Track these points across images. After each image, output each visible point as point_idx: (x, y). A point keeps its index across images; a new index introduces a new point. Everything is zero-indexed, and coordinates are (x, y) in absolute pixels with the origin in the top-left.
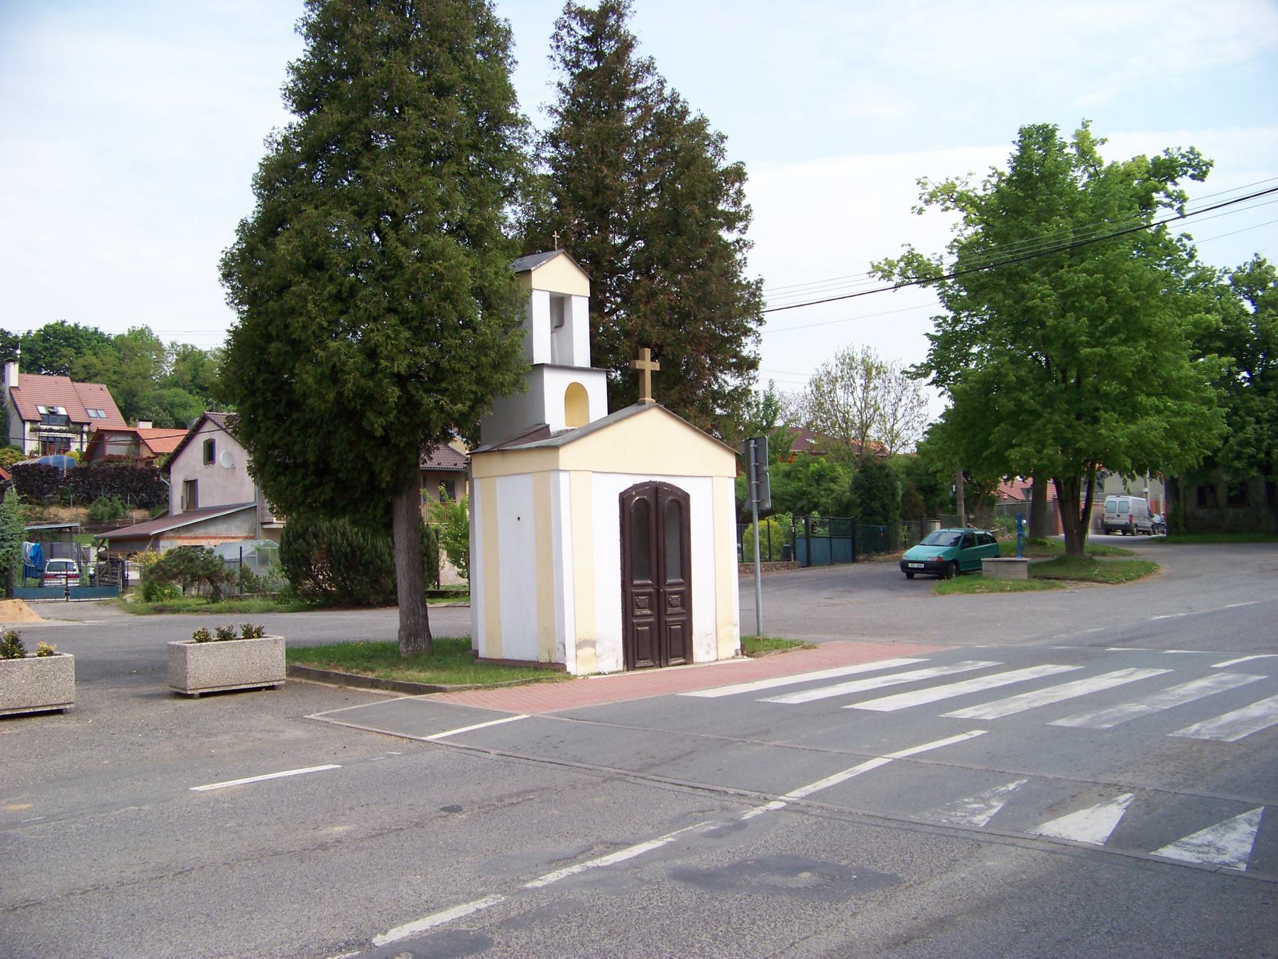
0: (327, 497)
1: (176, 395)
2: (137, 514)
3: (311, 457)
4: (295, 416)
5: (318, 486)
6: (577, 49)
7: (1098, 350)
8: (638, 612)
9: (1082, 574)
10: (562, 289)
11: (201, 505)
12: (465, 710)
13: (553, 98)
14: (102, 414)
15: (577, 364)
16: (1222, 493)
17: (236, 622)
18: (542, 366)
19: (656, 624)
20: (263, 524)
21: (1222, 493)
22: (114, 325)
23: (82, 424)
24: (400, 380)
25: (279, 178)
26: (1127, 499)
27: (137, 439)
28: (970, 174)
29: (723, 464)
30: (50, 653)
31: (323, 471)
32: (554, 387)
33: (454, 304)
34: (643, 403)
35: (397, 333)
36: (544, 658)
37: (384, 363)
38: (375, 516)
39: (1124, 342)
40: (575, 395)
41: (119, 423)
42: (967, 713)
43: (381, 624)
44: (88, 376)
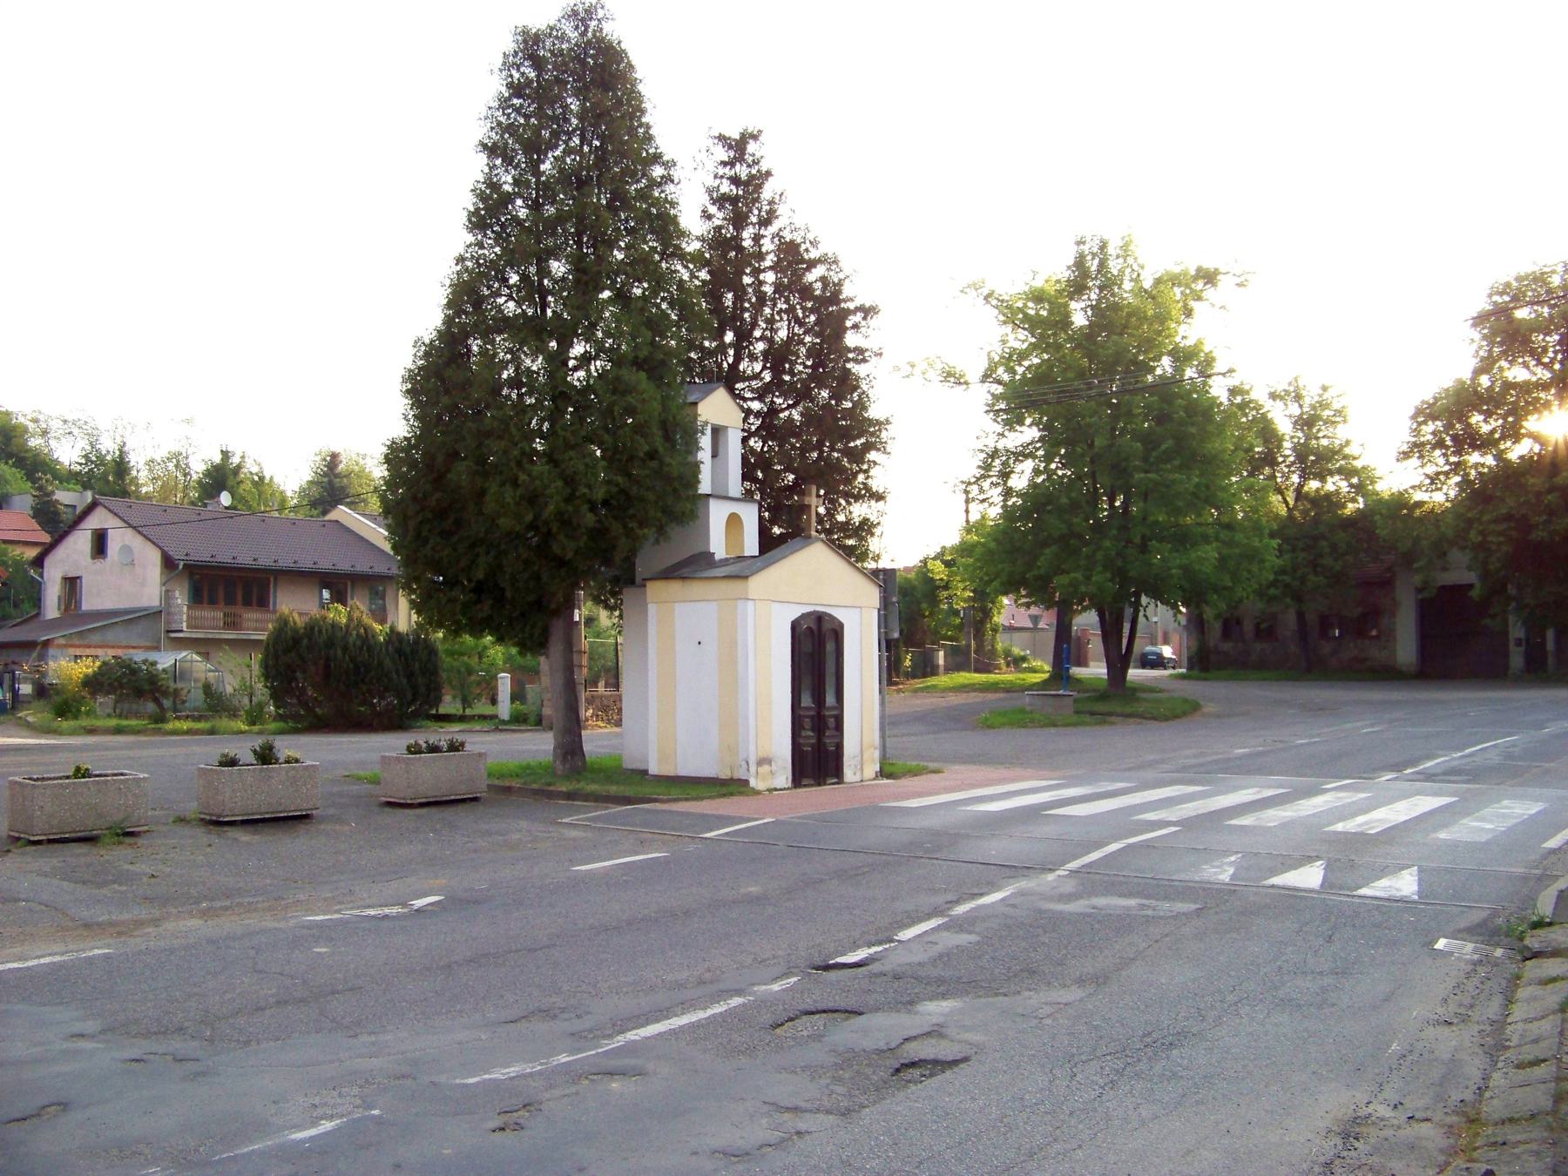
0: (485, 615)
7: (1152, 476)
9: (1128, 710)
11: (85, 606)
12: (704, 816)
15: (731, 494)
16: (1248, 627)
21: (1248, 627)
25: (468, 295)
26: (1163, 631)
29: (871, 596)
30: (297, 761)
32: (718, 514)
34: (809, 537)
36: (725, 774)
38: (531, 635)
39: (1180, 468)
40: (734, 521)
42: (1151, 816)
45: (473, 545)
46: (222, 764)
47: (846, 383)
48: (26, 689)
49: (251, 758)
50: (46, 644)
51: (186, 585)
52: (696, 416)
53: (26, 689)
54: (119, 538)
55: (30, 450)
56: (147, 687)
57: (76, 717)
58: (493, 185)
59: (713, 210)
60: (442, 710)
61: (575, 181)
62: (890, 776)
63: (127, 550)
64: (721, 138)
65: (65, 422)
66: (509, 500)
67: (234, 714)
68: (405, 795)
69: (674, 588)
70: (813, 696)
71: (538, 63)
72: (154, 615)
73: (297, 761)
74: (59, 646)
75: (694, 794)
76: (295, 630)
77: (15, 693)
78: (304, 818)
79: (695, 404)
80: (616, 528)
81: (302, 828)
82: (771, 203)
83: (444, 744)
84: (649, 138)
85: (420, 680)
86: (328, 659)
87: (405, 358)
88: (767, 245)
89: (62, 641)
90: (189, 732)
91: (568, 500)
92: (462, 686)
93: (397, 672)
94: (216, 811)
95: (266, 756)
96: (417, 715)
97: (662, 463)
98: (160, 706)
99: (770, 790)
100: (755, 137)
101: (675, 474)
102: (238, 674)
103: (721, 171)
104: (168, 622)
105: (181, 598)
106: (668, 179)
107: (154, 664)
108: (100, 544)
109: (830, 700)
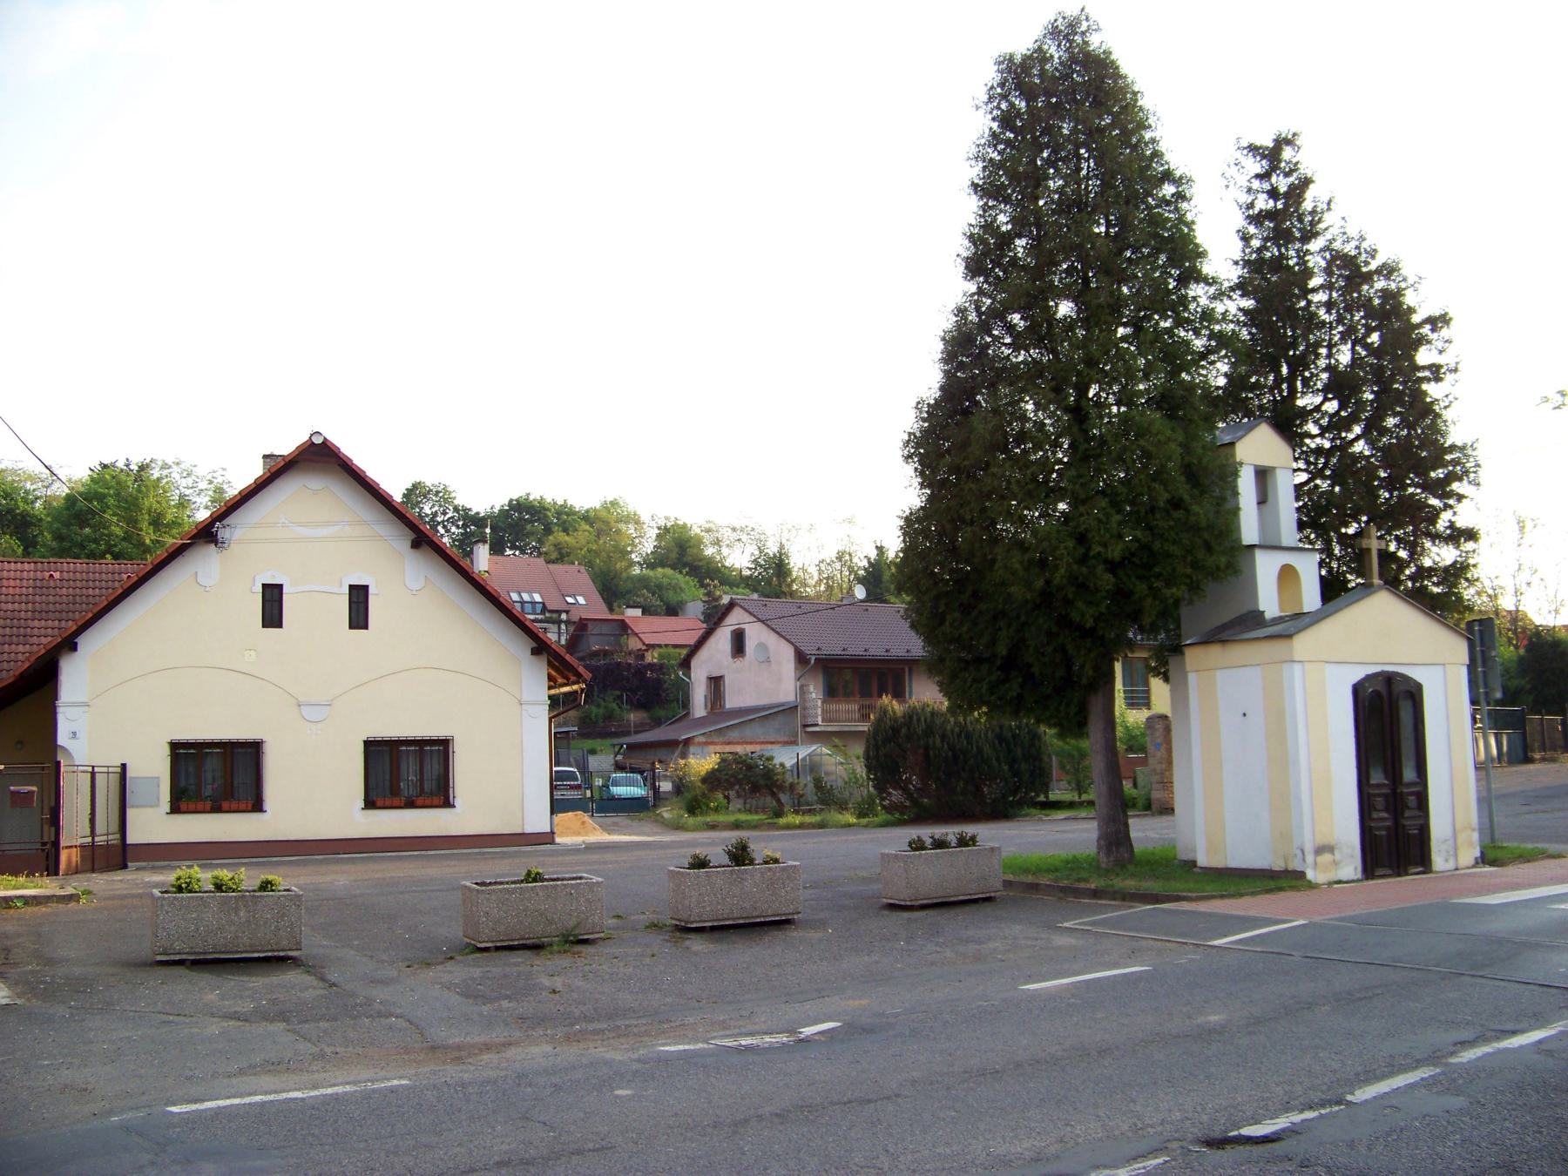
1: (664, 576)
2: (633, 717)
3: (1002, 650)
4: (982, 606)
5: (1004, 682)
6: (1249, 190)
8: (1375, 815)
10: (1265, 462)
11: (728, 706)
12: (1226, 917)
13: (1236, 249)
14: (581, 600)
15: (1285, 543)
17: (950, 832)
18: (1252, 547)
19: (1394, 833)
20: (806, 726)
22: (583, 498)
23: (559, 612)
24: (1112, 567)
25: (963, 346)
27: (623, 627)
28: (273, 599)
29: (1456, 651)
31: (1010, 664)
32: (1266, 567)
33: (1164, 484)
35: (1107, 516)
36: (1278, 865)
37: (1097, 549)
40: (1287, 575)
41: (600, 611)
43: (1062, 836)
44: (562, 556)
45: (995, 618)
46: (692, 866)
47: (1422, 412)
48: (666, 786)
49: (726, 860)
50: (687, 742)
51: (820, 679)
52: (1233, 455)
53: (666, 786)
54: (756, 635)
55: (705, 558)
56: (762, 782)
57: (702, 814)
58: (989, 227)
59: (1252, 230)
60: (1053, 797)
61: (1074, 206)
62: (1493, 863)
63: (762, 647)
64: (1253, 149)
65: (734, 529)
66: (1017, 566)
67: (842, 807)
68: (903, 897)
69: (1214, 653)
70: (1385, 772)
71: (1029, 94)
72: (791, 710)
73: (776, 861)
74: (699, 744)
75: (1232, 889)
76: (895, 719)
77: (656, 790)
78: (783, 924)
79: (1232, 444)
80: (1141, 588)
81: (778, 935)
82: (1313, 212)
83: (952, 839)
84: (1157, 154)
85: (1024, 766)
86: (927, 749)
87: (908, 422)
88: (1316, 262)
89: (702, 739)
90: (801, 826)
91: (1083, 560)
92: (1077, 770)
93: (998, 759)
94: (685, 917)
95: (740, 856)
96: (1020, 804)
97: (1187, 510)
98: (779, 801)
99: (1330, 884)
100: (1288, 142)
101: (1203, 524)
102: (844, 765)
103: (1256, 184)
104: (804, 717)
105: (815, 693)
106: (1180, 196)
107: (770, 759)
108: (738, 644)
109: (1409, 774)
